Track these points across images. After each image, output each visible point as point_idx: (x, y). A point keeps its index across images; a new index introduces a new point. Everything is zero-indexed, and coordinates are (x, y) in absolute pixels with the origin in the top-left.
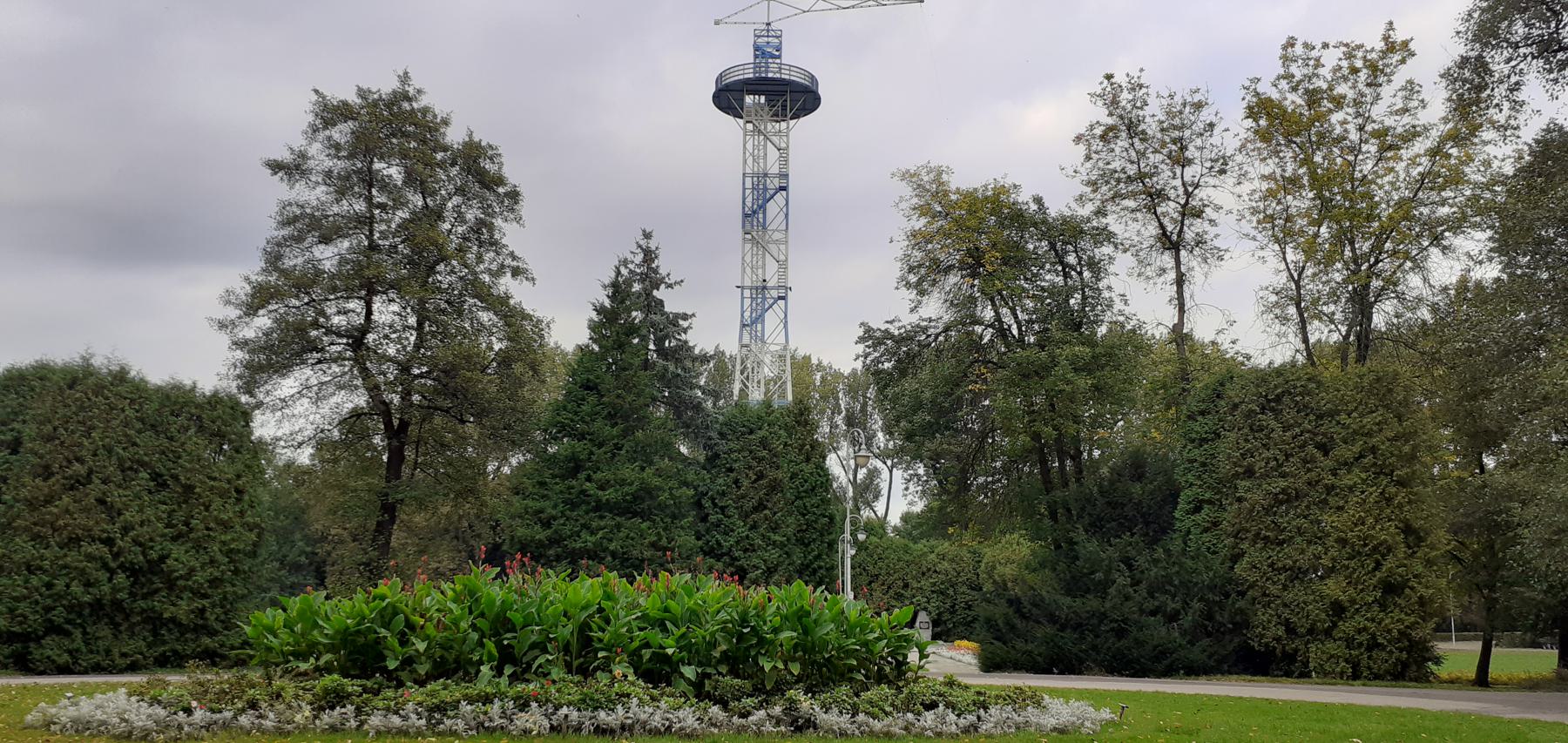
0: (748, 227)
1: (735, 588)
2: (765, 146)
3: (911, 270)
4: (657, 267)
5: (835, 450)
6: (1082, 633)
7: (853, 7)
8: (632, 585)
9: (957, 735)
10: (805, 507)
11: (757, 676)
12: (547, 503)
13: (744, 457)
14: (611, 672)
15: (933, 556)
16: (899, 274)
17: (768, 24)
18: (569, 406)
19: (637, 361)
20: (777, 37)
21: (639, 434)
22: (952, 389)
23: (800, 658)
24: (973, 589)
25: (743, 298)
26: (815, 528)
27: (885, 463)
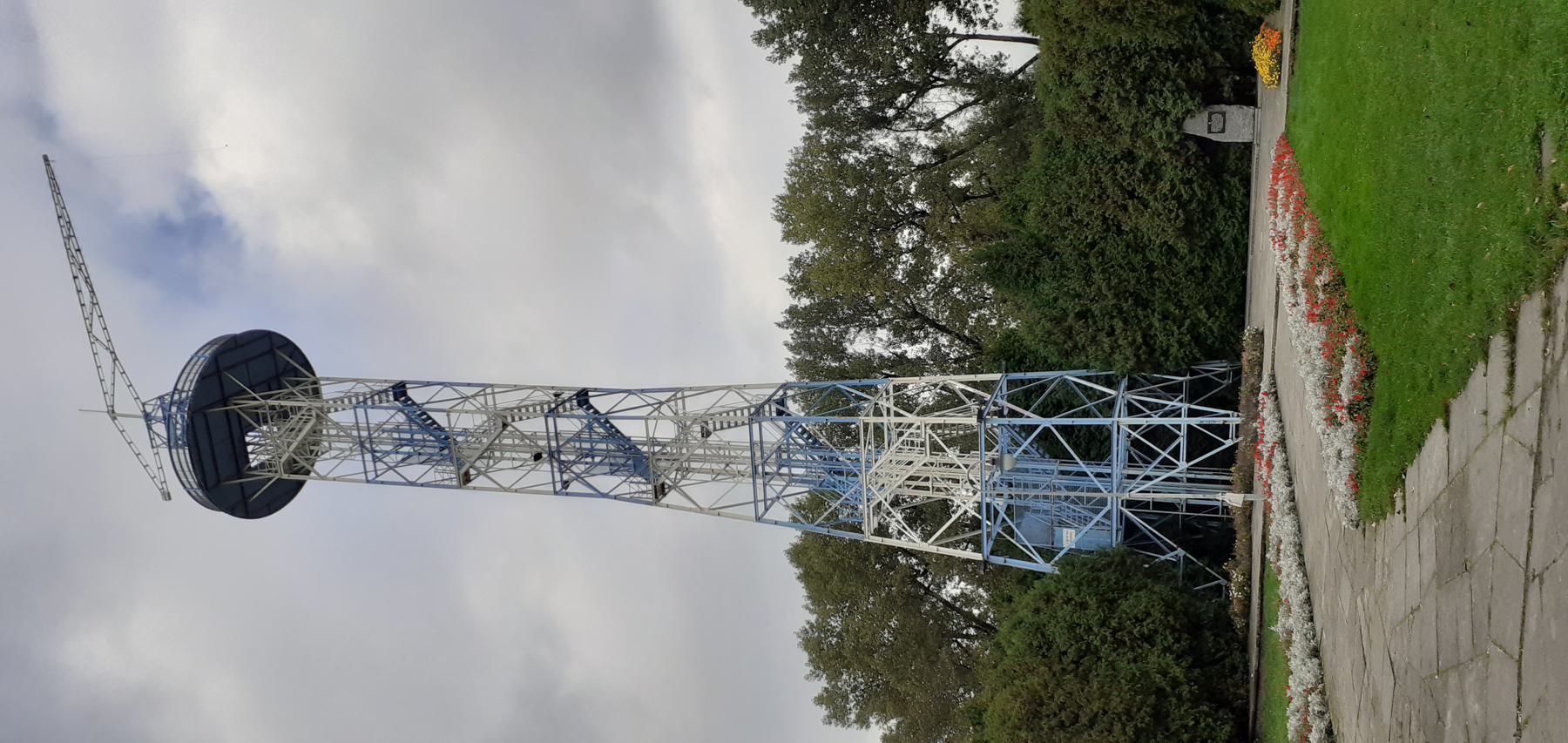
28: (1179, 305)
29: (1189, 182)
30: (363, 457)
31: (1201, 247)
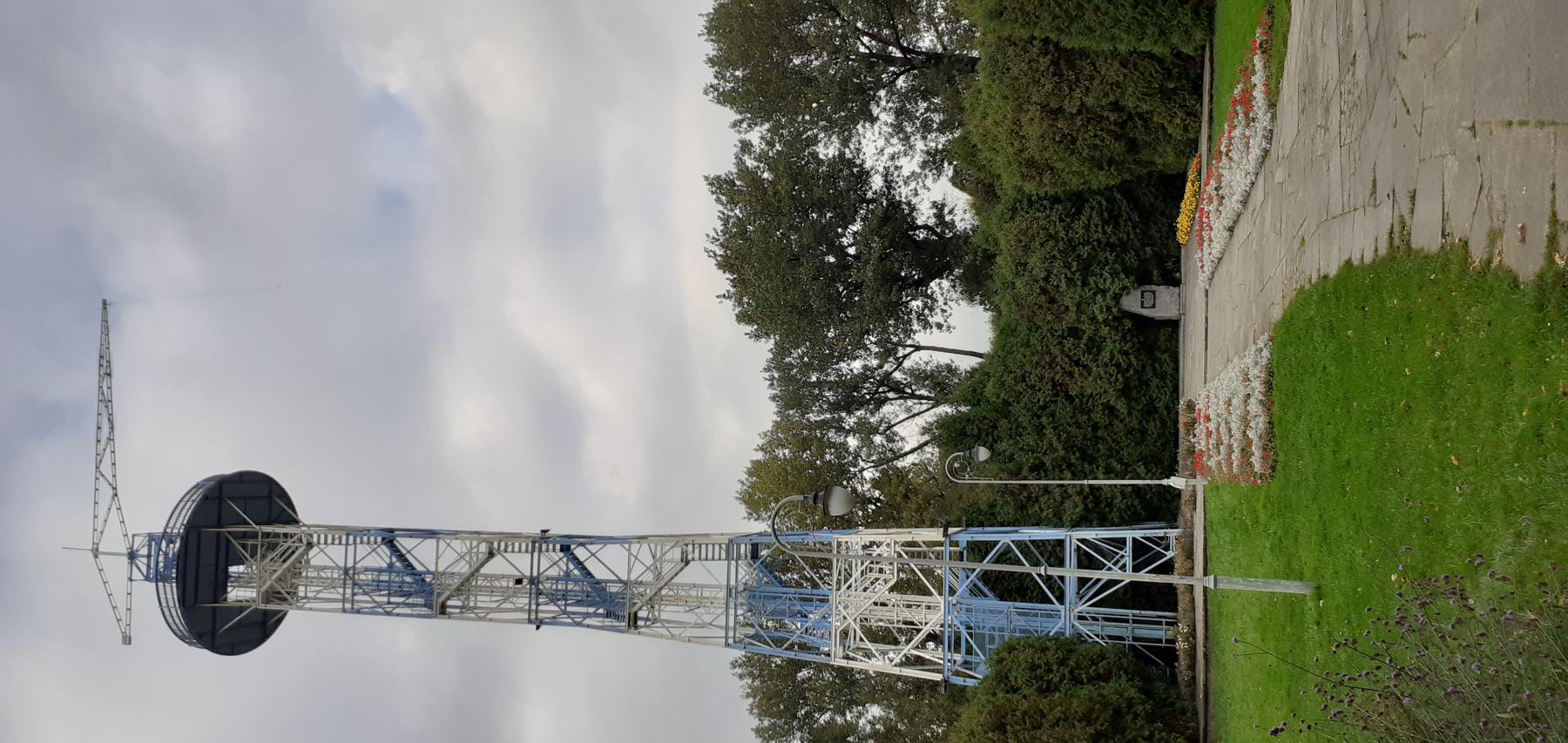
15: (1018, 284)
24: (1079, 212)
28: (1120, 461)
29: (1126, 353)
30: (344, 591)
31: (1138, 411)
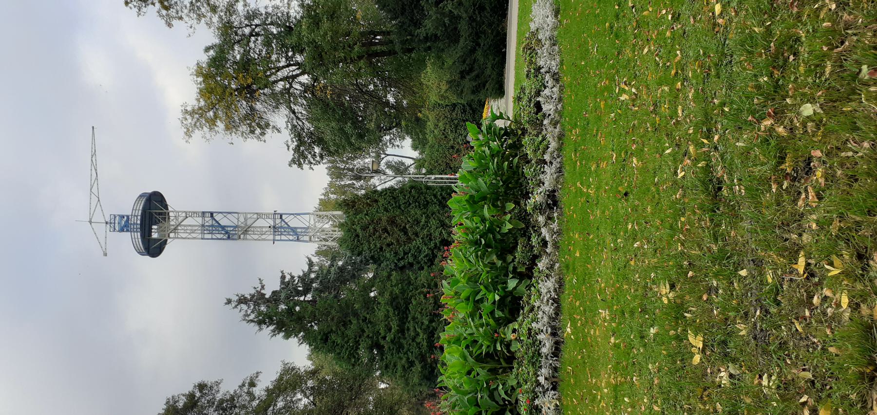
0: (236, 237)
1: (453, 249)
2: (185, 226)
3: (252, 132)
4: (250, 295)
5: (375, 187)
6: (481, 32)
7: (96, 170)
8: (450, 323)
9: (560, 86)
10: (405, 203)
11: (515, 234)
12: (399, 363)
13: (373, 240)
14: (511, 341)
15: (436, 131)
16: (255, 140)
17: (107, 223)
18: (338, 351)
19: (310, 308)
20: (115, 217)
21: (357, 306)
22: (330, 109)
23: (502, 203)
24: (454, 109)
25: (281, 240)
26: (418, 198)
27: (383, 158)
